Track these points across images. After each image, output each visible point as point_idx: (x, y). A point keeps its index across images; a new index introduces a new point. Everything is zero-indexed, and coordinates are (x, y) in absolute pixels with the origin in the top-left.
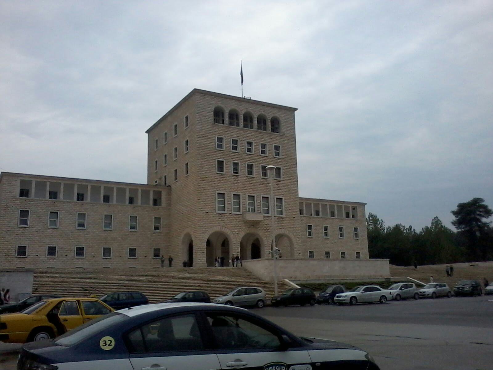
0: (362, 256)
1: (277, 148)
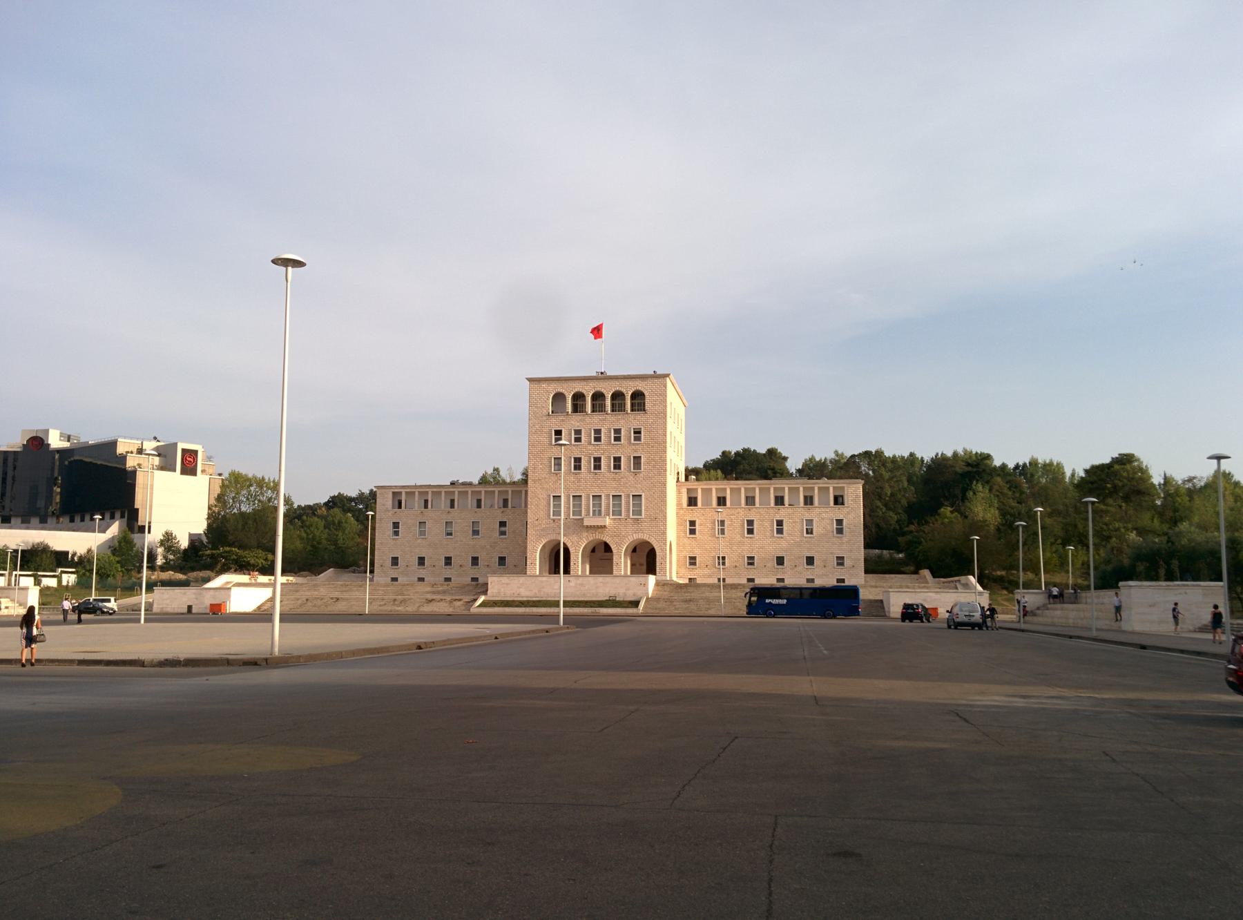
0: (847, 562)
1: (638, 432)
